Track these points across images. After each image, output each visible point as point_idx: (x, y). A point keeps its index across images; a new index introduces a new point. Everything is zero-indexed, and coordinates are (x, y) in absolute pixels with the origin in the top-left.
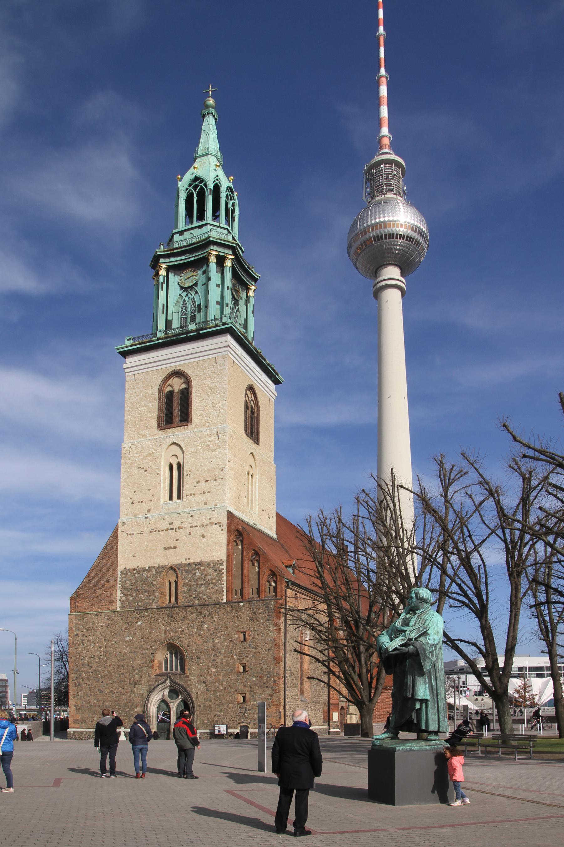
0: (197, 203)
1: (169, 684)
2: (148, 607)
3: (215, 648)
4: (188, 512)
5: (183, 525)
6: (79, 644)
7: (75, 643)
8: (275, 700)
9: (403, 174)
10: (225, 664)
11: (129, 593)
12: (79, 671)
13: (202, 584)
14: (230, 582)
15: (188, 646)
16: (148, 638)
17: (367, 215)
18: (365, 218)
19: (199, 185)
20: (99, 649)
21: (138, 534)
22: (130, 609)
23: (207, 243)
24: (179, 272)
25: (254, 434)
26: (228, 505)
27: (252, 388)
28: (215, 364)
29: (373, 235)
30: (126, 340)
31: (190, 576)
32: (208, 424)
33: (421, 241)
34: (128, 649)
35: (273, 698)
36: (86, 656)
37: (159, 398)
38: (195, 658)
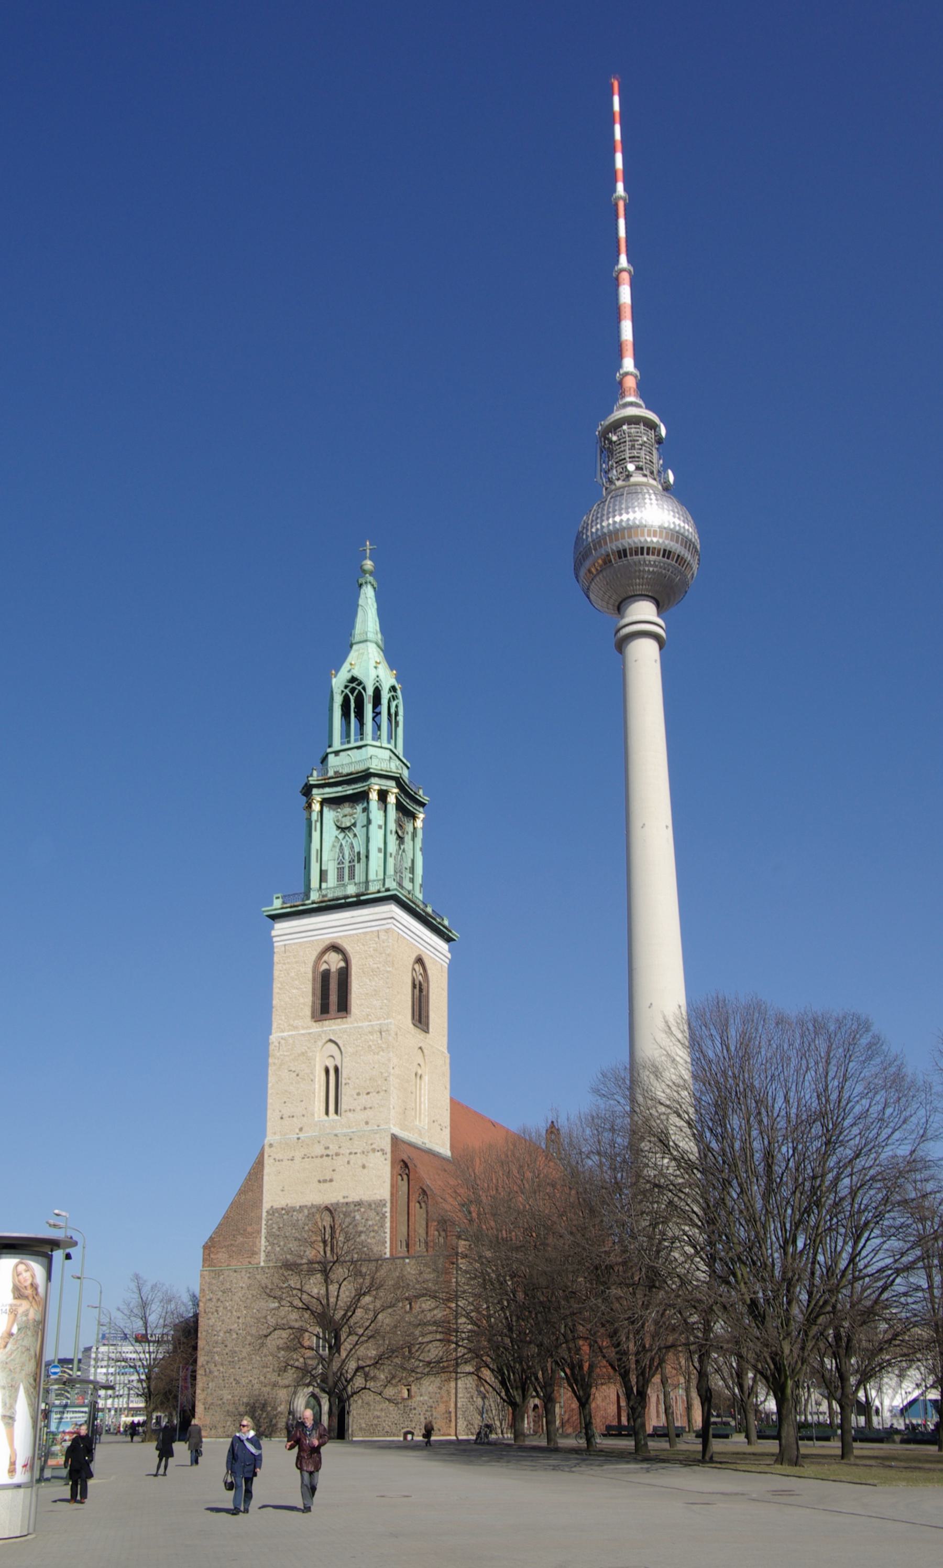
1: (321, 1371)
5: (341, 1151)
6: (212, 1313)
11: (275, 1242)
17: (603, 515)
19: (356, 689)
23: (366, 775)
24: (334, 806)
25: (423, 1019)
26: (392, 1126)
28: (377, 939)
33: (686, 555)
37: (314, 979)
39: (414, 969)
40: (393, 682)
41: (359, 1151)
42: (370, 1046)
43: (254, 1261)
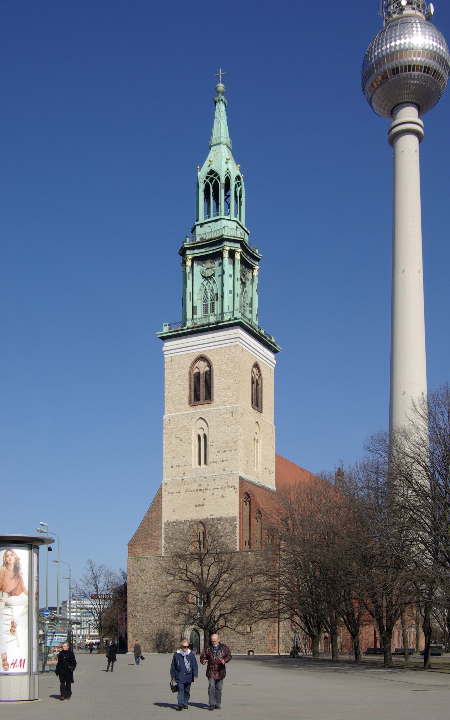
0: (213, 195)
4: (212, 477)
7: (132, 581)
8: (272, 631)
11: (170, 542)
14: (242, 535)
18: (380, 46)
20: (150, 587)
21: (177, 493)
22: (171, 554)
23: (221, 240)
24: (200, 262)
25: (259, 404)
26: (239, 472)
27: (257, 364)
28: (229, 352)
29: (388, 68)
30: (164, 326)
35: (271, 629)
36: (140, 593)
37: (190, 379)
41: (219, 487)
42: (225, 422)
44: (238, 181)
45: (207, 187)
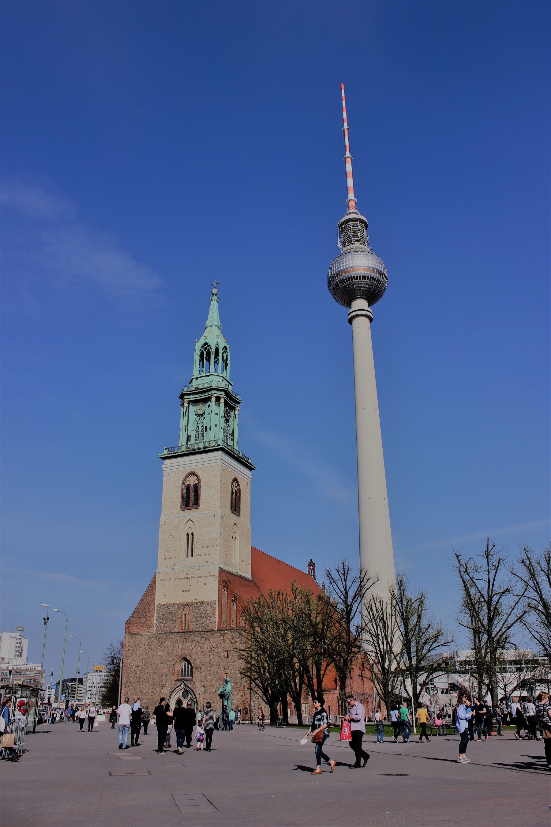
2: (172, 632)
3: (210, 662)
5: (194, 576)
6: (130, 657)
9: (366, 227)
10: (216, 673)
11: (161, 621)
12: (128, 676)
13: (203, 617)
15: (195, 660)
16: (171, 654)
18: (339, 264)
28: (213, 470)
31: (197, 611)
32: (209, 508)
34: (159, 661)
37: (182, 489)
38: (199, 669)
39: (232, 484)
40: (225, 344)
43: (151, 631)
44: (225, 350)
45: (202, 354)
